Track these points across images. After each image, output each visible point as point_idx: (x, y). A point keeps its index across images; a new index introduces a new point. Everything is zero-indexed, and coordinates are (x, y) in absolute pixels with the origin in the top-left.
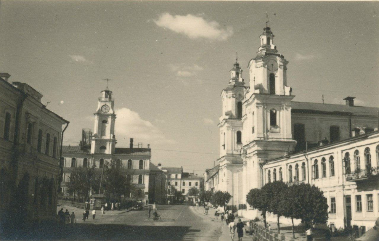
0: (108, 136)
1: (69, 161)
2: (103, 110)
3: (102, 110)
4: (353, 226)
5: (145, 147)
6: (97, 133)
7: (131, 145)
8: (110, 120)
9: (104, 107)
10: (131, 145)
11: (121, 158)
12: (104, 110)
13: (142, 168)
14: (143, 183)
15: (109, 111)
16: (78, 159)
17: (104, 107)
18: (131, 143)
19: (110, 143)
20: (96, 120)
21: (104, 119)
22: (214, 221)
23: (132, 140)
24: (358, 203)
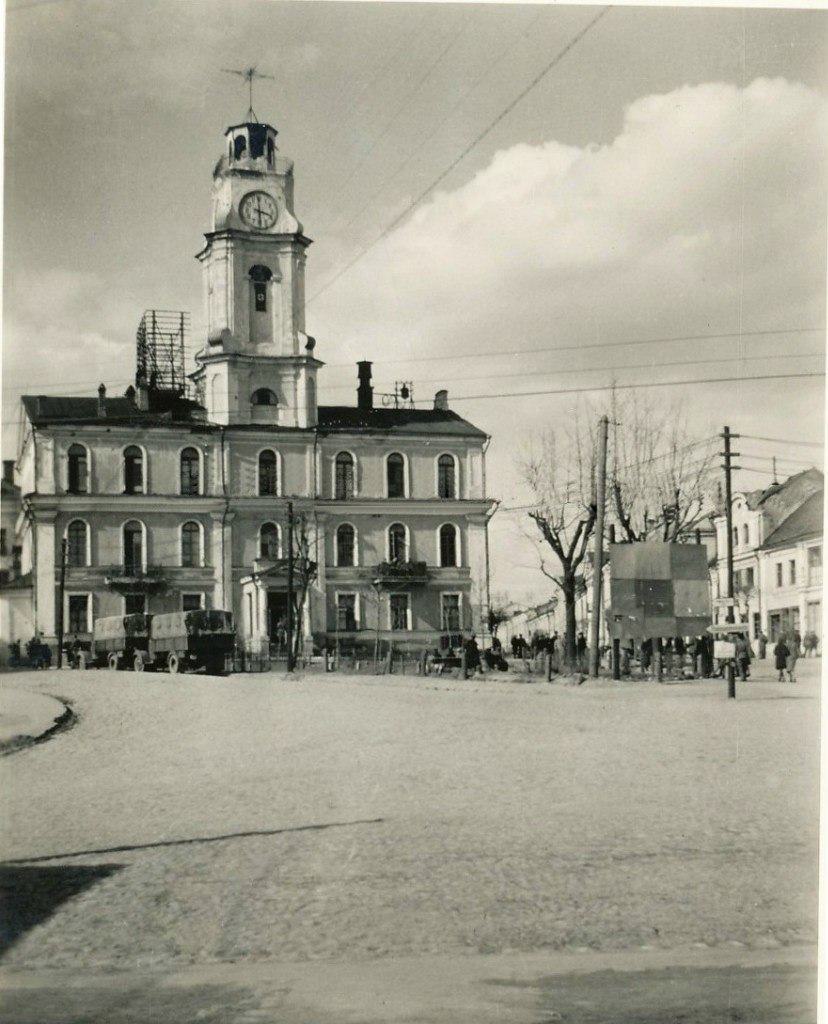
0: (280, 343)
1: (113, 459)
2: (249, 216)
3: (245, 215)
4: (391, 643)
5: (424, 401)
6: (232, 328)
7: (365, 392)
8: (285, 263)
9: (250, 200)
10: (365, 392)
11: (354, 450)
12: (254, 215)
13: (273, 492)
14: (459, 563)
15: (273, 224)
16: (98, 451)
17: (253, 203)
18: (368, 383)
19: (296, 376)
20: (220, 271)
21: (257, 258)
22: (680, 735)
23: (365, 369)
24: (756, 625)
